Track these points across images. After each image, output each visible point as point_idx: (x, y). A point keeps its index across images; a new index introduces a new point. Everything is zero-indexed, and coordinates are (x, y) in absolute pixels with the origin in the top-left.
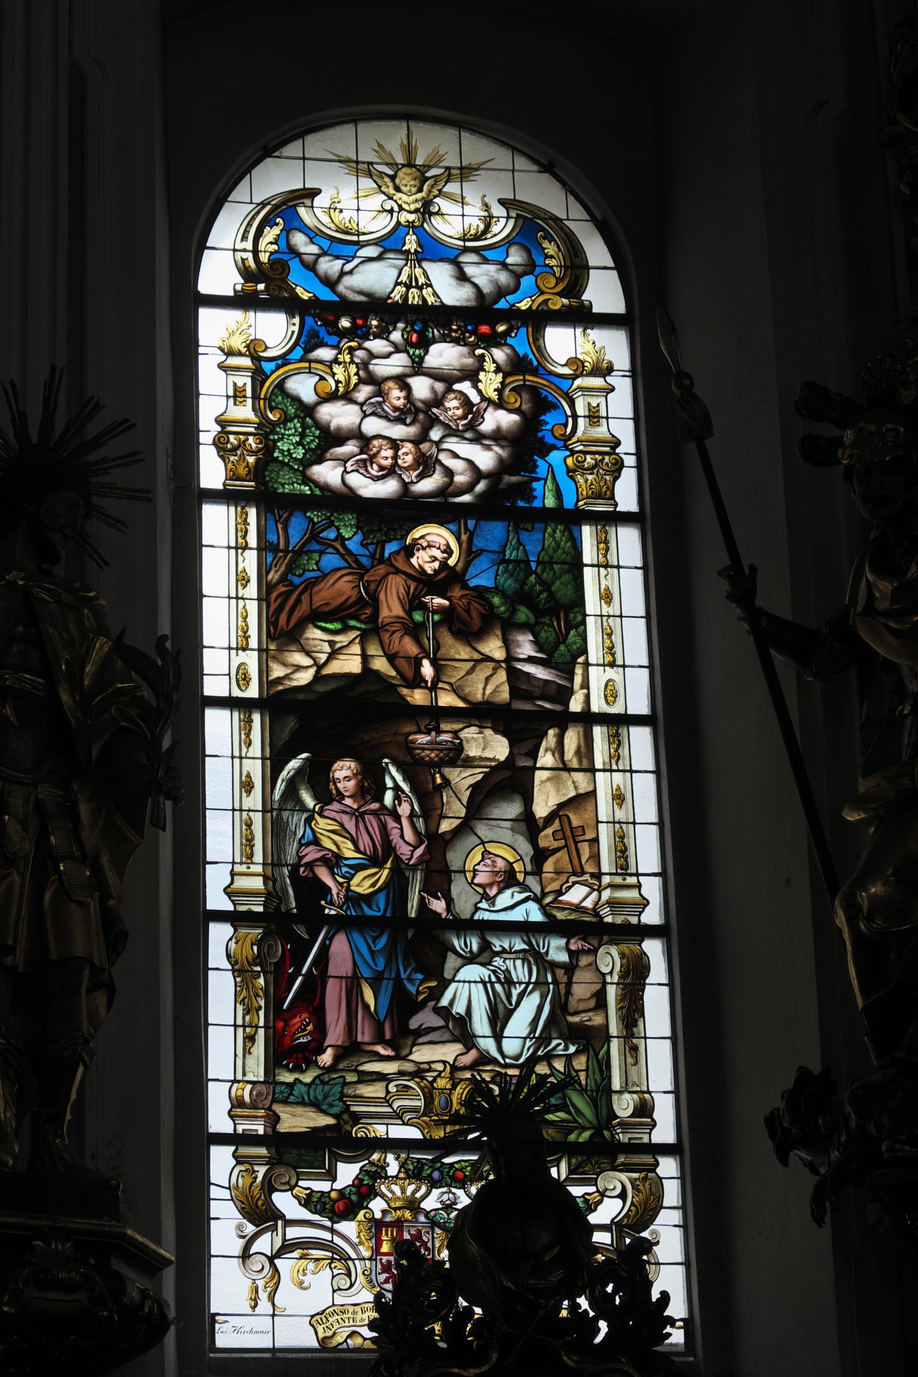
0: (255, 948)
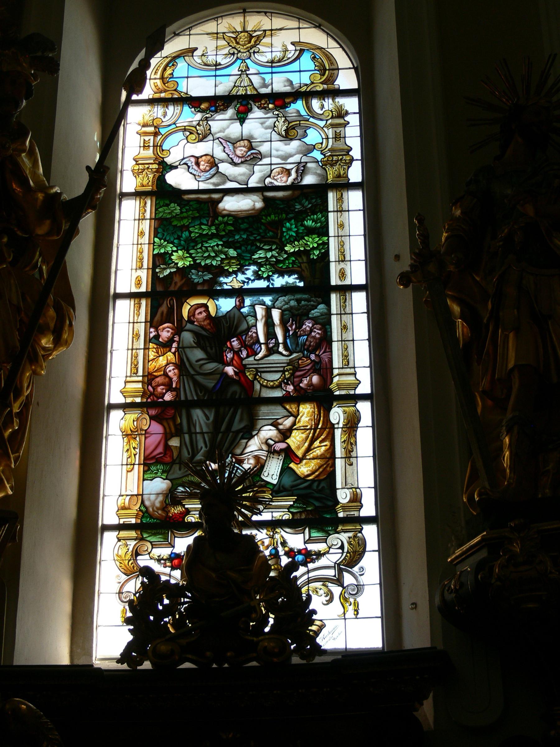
0: (135, 423)
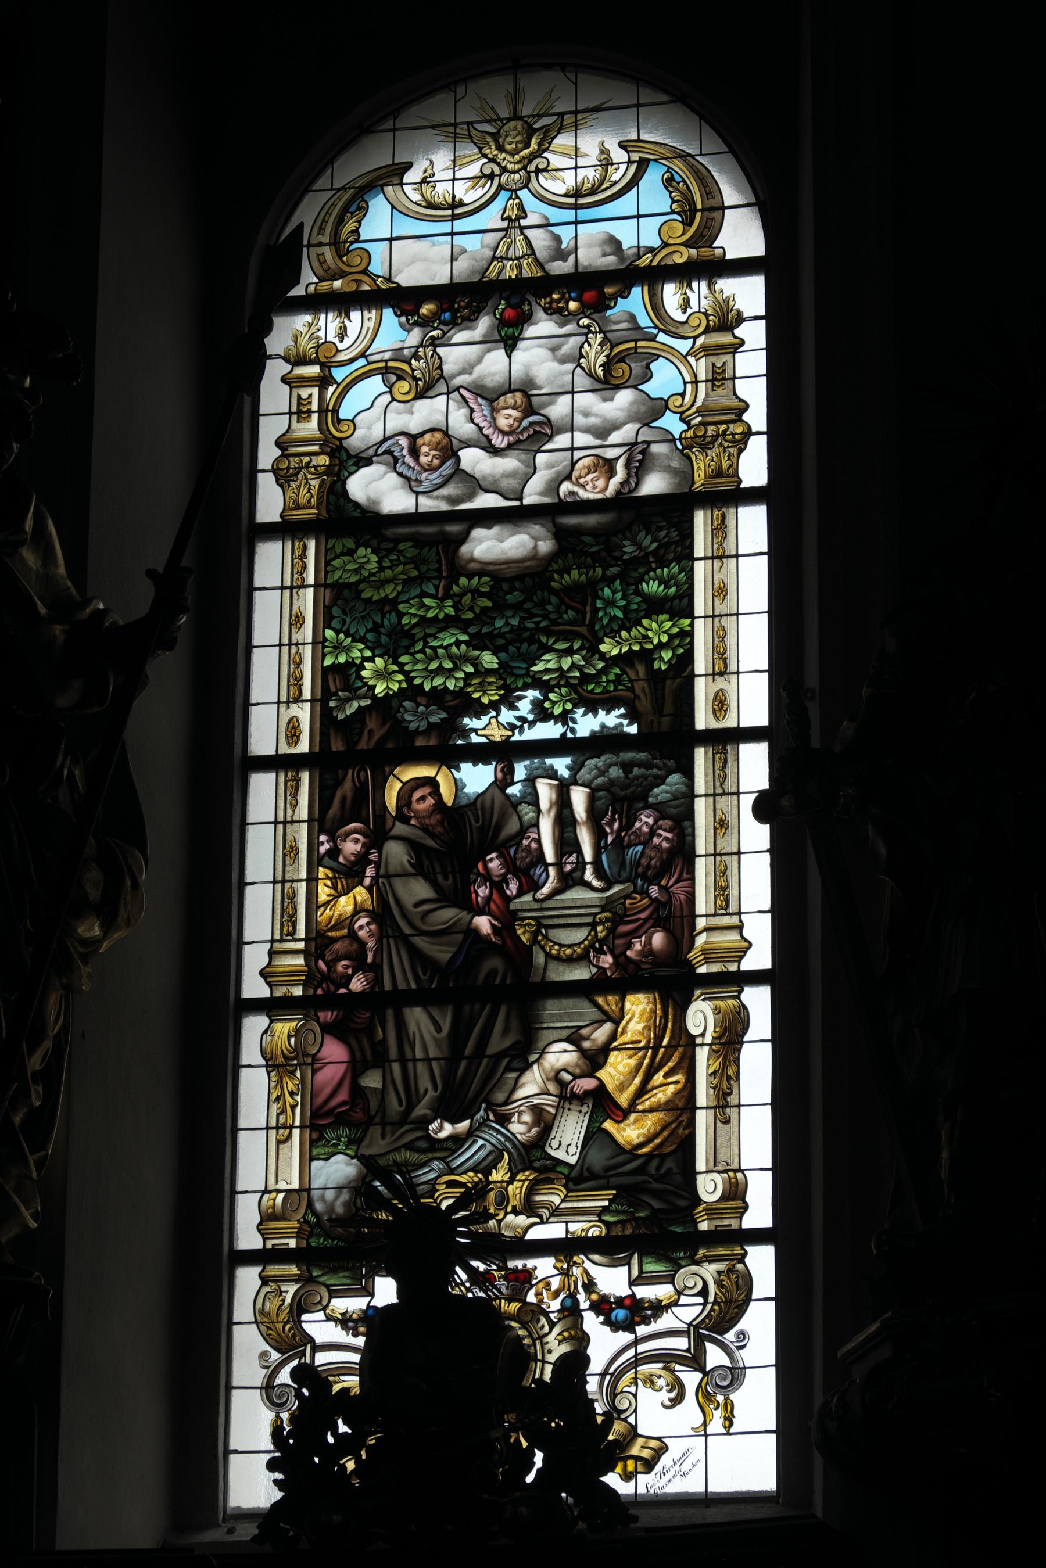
0: (293, 1040)
